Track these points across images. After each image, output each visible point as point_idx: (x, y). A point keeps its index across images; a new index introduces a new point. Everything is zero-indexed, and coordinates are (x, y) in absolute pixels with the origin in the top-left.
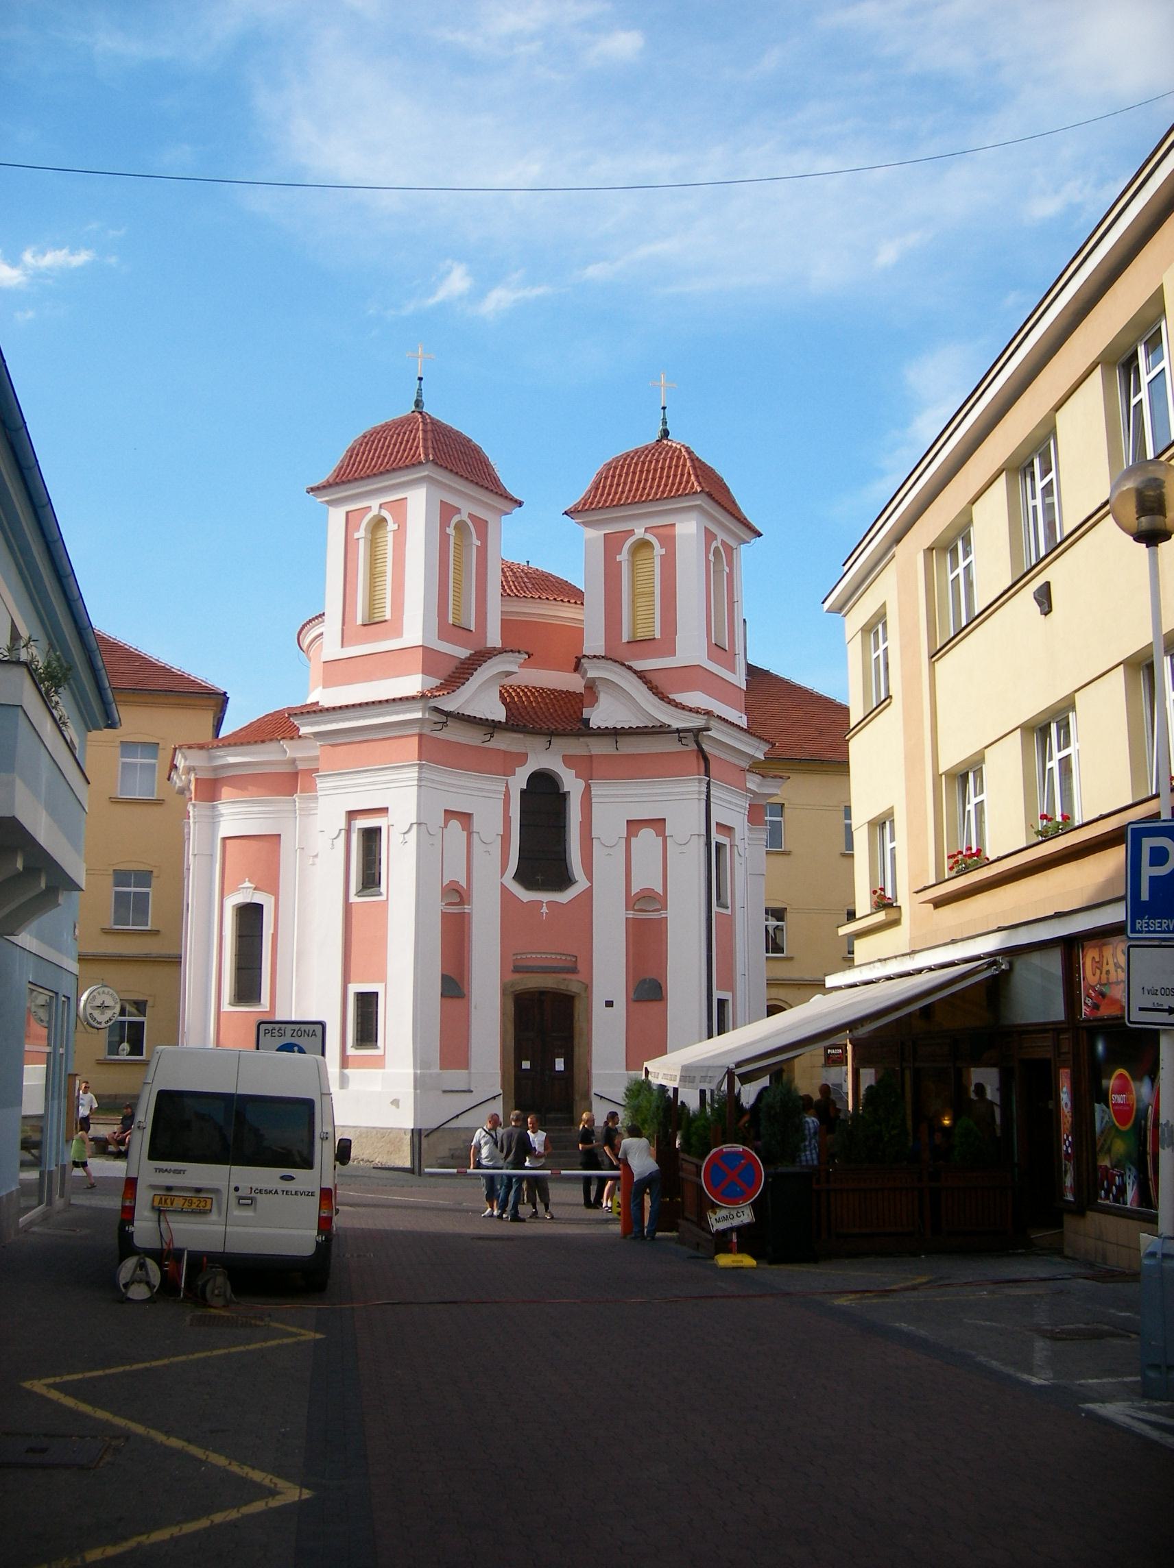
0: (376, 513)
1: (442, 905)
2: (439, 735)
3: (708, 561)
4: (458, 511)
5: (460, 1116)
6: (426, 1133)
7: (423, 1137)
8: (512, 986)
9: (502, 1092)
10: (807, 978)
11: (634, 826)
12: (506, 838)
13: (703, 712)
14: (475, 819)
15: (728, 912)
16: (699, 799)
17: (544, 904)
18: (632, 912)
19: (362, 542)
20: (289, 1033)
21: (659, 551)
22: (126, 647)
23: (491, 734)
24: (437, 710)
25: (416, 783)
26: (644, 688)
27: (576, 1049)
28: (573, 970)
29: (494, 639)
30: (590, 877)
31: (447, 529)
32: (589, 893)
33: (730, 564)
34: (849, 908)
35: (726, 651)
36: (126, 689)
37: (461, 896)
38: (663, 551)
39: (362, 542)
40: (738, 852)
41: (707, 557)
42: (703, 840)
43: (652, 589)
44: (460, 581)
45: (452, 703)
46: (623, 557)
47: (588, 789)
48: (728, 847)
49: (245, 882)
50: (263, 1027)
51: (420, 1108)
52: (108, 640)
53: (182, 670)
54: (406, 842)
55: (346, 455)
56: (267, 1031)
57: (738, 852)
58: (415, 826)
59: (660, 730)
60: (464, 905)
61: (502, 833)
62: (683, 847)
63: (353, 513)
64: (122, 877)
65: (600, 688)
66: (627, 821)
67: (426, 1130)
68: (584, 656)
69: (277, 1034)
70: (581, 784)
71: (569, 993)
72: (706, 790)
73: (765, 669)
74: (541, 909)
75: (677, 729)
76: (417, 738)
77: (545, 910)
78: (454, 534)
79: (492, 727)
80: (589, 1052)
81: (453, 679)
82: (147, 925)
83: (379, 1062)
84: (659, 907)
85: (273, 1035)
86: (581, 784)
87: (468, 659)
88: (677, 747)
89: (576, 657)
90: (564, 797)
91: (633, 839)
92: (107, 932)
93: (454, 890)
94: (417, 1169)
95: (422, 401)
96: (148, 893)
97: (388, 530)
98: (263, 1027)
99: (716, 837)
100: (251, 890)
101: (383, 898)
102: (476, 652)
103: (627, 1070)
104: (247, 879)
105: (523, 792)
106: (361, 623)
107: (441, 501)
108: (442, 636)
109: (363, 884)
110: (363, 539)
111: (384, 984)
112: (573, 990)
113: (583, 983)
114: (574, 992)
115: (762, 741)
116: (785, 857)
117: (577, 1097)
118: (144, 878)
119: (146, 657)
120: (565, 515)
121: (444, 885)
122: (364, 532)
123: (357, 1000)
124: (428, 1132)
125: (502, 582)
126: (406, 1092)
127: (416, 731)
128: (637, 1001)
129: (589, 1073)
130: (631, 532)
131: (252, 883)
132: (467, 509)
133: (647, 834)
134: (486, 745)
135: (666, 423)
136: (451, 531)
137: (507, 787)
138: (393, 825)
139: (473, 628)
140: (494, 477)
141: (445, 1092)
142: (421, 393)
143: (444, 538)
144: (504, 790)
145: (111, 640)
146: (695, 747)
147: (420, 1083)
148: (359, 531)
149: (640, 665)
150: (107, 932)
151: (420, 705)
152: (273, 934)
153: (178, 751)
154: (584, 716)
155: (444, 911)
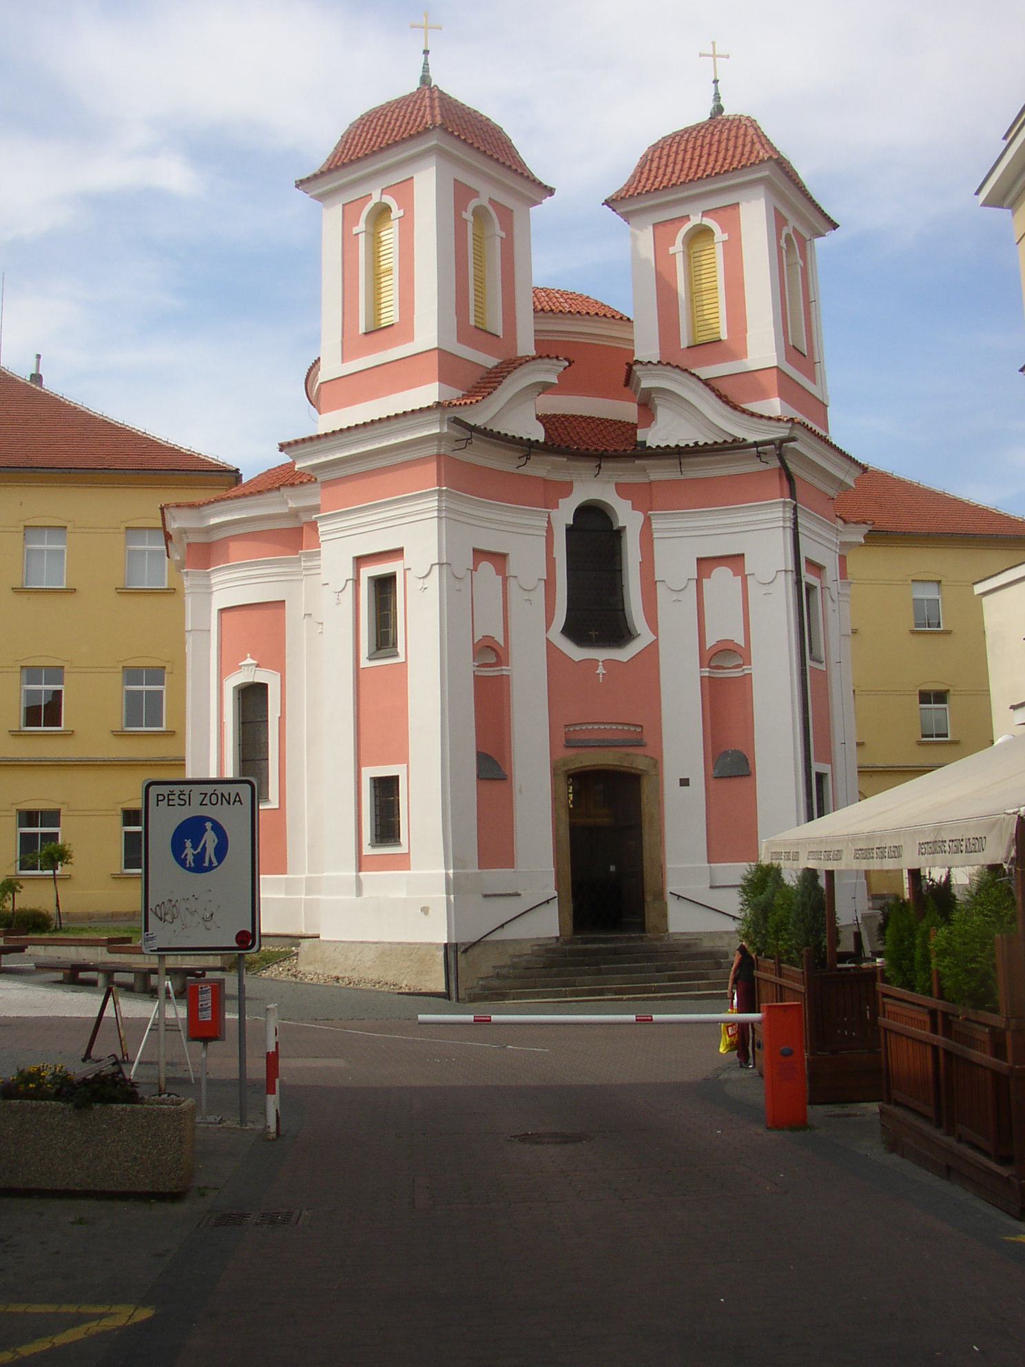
0: (378, 200)
1: (474, 665)
2: (459, 455)
3: (780, 248)
4: (475, 194)
5: (505, 926)
6: (463, 948)
8: (564, 764)
9: (557, 895)
11: (706, 564)
12: (550, 584)
13: (785, 419)
15: (369, 772)
16: (784, 527)
17: (600, 664)
18: (708, 669)
19: (362, 238)
20: (197, 799)
21: (720, 236)
22: (134, 431)
23: (527, 455)
24: (457, 421)
25: (436, 514)
26: (712, 398)
28: (640, 744)
29: (526, 346)
30: (656, 632)
31: (463, 213)
32: (653, 648)
33: (804, 257)
34: (922, 689)
35: (804, 356)
36: (129, 469)
37: (497, 655)
38: (725, 237)
40: (831, 598)
41: (778, 243)
42: (791, 578)
43: (714, 283)
45: (479, 417)
47: (648, 521)
48: (819, 589)
49: (246, 658)
50: (154, 790)
51: (456, 914)
52: (115, 426)
53: (192, 450)
54: (425, 588)
55: (341, 141)
56: (161, 798)
57: (831, 598)
58: (436, 568)
59: (733, 446)
61: (545, 578)
64: (132, 674)
65: (657, 401)
66: (700, 560)
67: (463, 944)
68: (637, 362)
69: (177, 801)
70: (639, 517)
75: (755, 442)
76: (434, 465)
77: (601, 670)
79: (528, 448)
80: (660, 843)
81: (477, 390)
82: (161, 726)
83: (403, 862)
84: (742, 663)
85: (171, 803)
86: (639, 517)
87: (496, 367)
89: (627, 364)
90: (618, 534)
91: (705, 580)
92: (118, 734)
93: (488, 647)
94: (453, 994)
95: (429, 76)
96: (162, 691)
97: (392, 218)
98: (154, 790)
99: (807, 577)
100: (254, 667)
101: (401, 659)
103: (709, 862)
104: (249, 655)
105: (569, 530)
106: (364, 331)
107: (455, 180)
108: (461, 339)
109: (377, 645)
110: (364, 234)
111: (406, 765)
113: (652, 758)
114: (641, 770)
115: (853, 465)
117: (649, 898)
118: (156, 675)
119: (155, 439)
120: (605, 206)
121: (476, 642)
122: (364, 225)
123: (375, 787)
124: (467, 946)
125: (534, 303)
126: (438, 897)
127: (434, 451)
129: (661, 868)
131: (254, 660)
132: (486, 193)
133: (722, 574)
134: (523, 471)
135: (720, 98)
136: (468, 215)
137: (549, 522)
138: (410, 569)
139: (500, 333)
140: (519, 161)
141: (486, 896)
142: (428, 69)
143: (460, 225)
144: (546, 525)
145: (119, 425)
146: (777, 464)
147: (455, 886)
148: (358, 224)
149: (706, 372)
150: (118, 734)
151: (437, 415)
153: (165, 510)
154: (639, 439)
155: (476, 674)
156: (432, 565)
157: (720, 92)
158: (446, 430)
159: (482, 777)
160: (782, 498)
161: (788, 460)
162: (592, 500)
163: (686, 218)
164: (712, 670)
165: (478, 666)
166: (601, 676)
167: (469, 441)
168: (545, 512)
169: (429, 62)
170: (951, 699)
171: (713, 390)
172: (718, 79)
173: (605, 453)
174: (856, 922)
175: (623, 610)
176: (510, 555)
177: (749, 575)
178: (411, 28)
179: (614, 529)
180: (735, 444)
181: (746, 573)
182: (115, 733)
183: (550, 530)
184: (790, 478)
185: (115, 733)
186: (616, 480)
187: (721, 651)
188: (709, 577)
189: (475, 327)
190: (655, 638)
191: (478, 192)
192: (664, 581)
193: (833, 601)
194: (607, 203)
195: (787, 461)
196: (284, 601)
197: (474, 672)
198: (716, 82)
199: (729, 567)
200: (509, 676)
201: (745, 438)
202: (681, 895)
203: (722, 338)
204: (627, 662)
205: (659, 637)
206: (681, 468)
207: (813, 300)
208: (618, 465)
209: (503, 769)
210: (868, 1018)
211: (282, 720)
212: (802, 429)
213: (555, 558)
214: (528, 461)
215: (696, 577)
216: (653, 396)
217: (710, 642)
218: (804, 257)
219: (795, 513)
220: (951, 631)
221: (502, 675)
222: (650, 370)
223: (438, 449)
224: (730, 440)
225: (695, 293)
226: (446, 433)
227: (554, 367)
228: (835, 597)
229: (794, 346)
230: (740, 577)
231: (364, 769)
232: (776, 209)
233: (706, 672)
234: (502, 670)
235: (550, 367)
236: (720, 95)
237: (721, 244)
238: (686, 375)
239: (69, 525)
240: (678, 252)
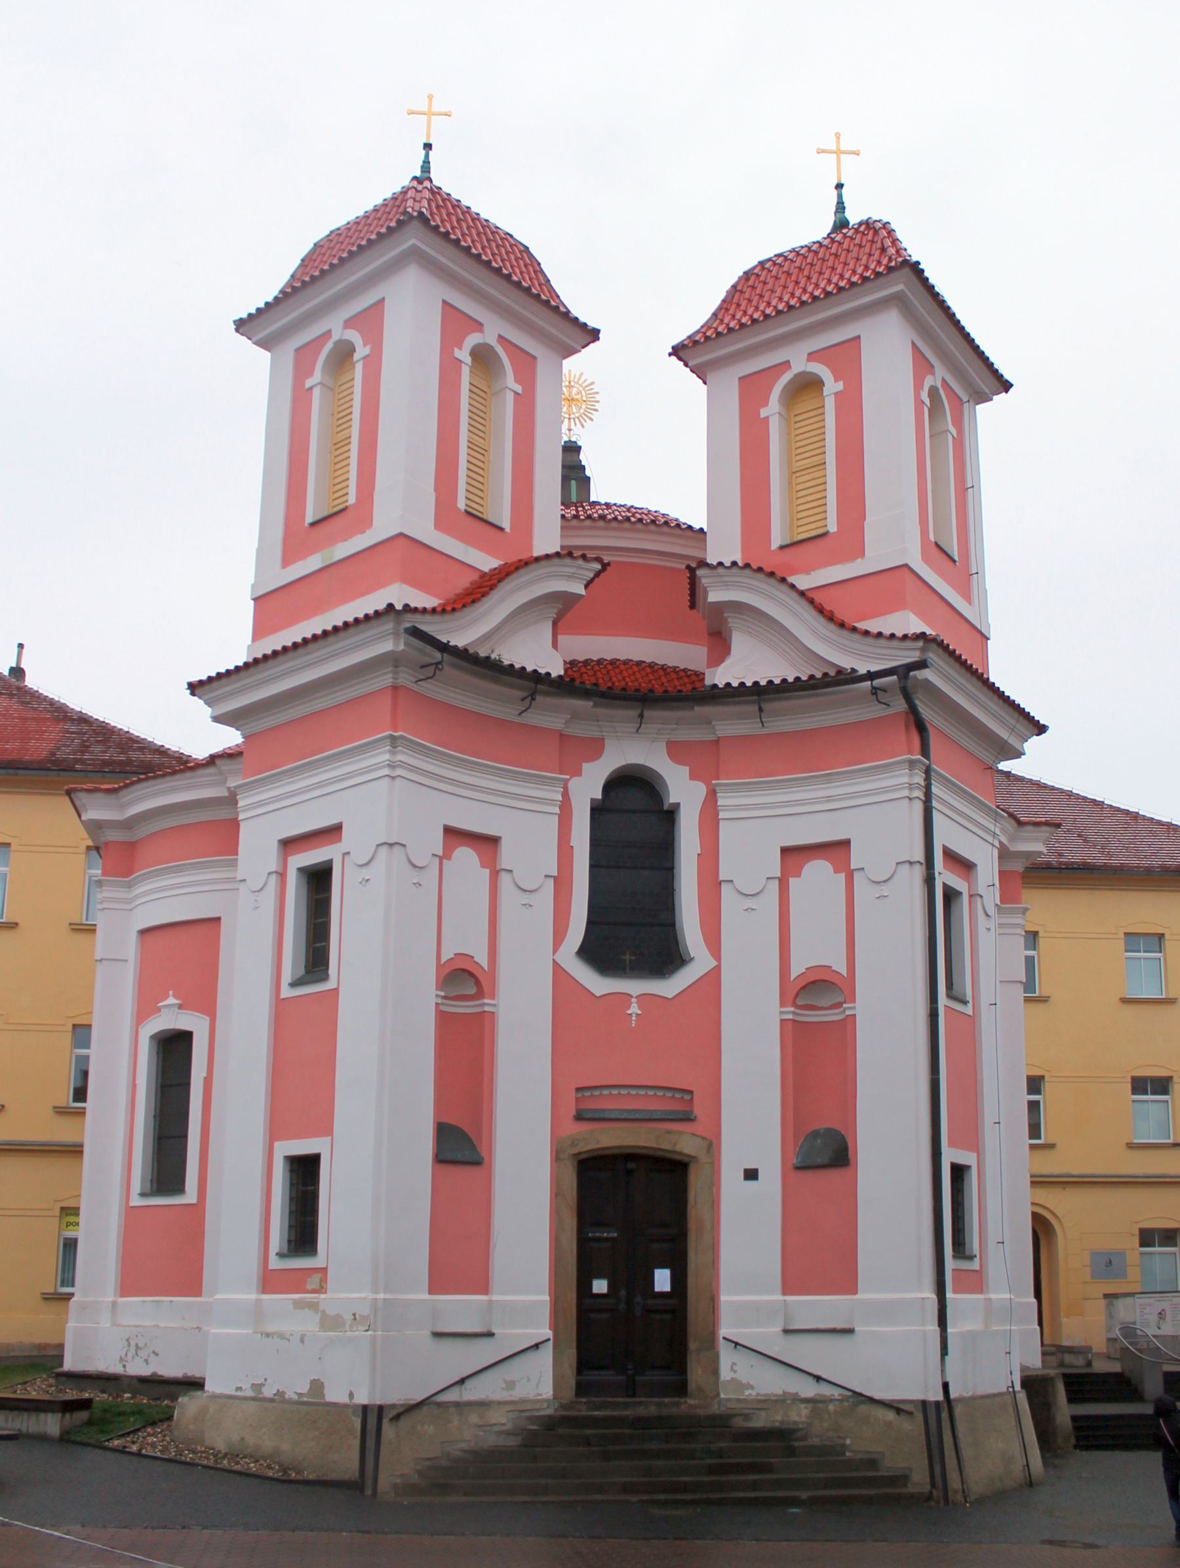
4: (479, 326)
6: (393, 1413)
8: (573, 1145)
10: (1074, 1172)
12: (562, 883)
14: (505, 848)
15: (975, 1265)
17: (634, 1000)
18: (792, 1009)
21: (832, 386)
24: (416, 633)
27: (691, 1255)
28: (687, 1118)
30: (717, 955)
31: (456, 350)
32: (713, 978)
35: (954, 561)
39: (316, 393)
42: (918, 872)
46: (772, 409)
47: (712, 795)
59: (845, 678)
60: (483, 997)
61: (556, 874)
63: (819, 1161)
66: (785, 851)
67: (393, 1406)
70: (700, 789)
72: (923, 783)
74: (629, 1009)
77: (634, 1009)
78: (470, 363)
80: (715, 1263)
84: (843, 1000)
86: (700, 789)
88: (874, 711)
90: (670, 816)
91: (793, 881)
99: (945, 876)
104: (171, 993)
105: (598, 811)
107: (445, 302)
108: (441, 523)
112: (685, 1151)
113: (703, 1138)
115: (1021, 718)
116: (1040, 1006)
117: (692, 1345)
128: (798, 1168)
129: (713, 1300)
130: (786, 365)
132: (493, 330)
133: (818, 870)
135: (844, 208)
137: (565, 794)
139: (506, 525)
141: (438, 1335)
149: (803, 582)
152: (205, 1078)
155: (442, 1008)
157: (844, 200)
158: (402, 647)
159: (441, 1159)
160: (908, 754)
161: (919, 699)
162: (631, 765)
163: (786, 365)
164: (798, 1011)
165: (445, 997)
166: (634, 1018)
167: (440, 666)
168: (559, 779)
169: (430, 160)
171: (811, 601)
172: (842, 182)
173: (649, 695)
174: (1011, 1390)
175: (673, 925)
177: (855, 870)
178: (409, 114)
180: (842, 677)
181: (852, 868)
182: (58, 1110)
184: (921, 727)
185: (58, 1110)
186: (668, 736)
187: (813, 982)
188: (799, 875)
189: (467, 512)
190: (715, 963)
191: (481, 325)
192: (732, 881)
193: (988, 915)
194: (677, 351)
195: (917, 702)
197: (437, 1004)
199: (826, 859)
200: (493, 1013)
201: (856, 668)
202: (740, 1342)
206: (761, 718)
207: (970, 485)
208: (668, 714)
209: (478, 1150)
211: (208, 1082)
212: (940, 651)
213: (572, 847)
215: (779, 875)
216: (725, 615)
217: (797, 969)
218: (958, 422)
219: (928, 779)
221: (484, 1011)
223: (394, 678)
224: (832, 673)
225: (794, 473)
226: (403, 650)
227: (581, 572)
229: (937, 544)
230: (843, 875)
231: (277, 1144)
232: (914, 344)
233: (789, 1012)
236: (845, 205)
237: (833, 396)
238: (784, 588)
239: (14, 842)
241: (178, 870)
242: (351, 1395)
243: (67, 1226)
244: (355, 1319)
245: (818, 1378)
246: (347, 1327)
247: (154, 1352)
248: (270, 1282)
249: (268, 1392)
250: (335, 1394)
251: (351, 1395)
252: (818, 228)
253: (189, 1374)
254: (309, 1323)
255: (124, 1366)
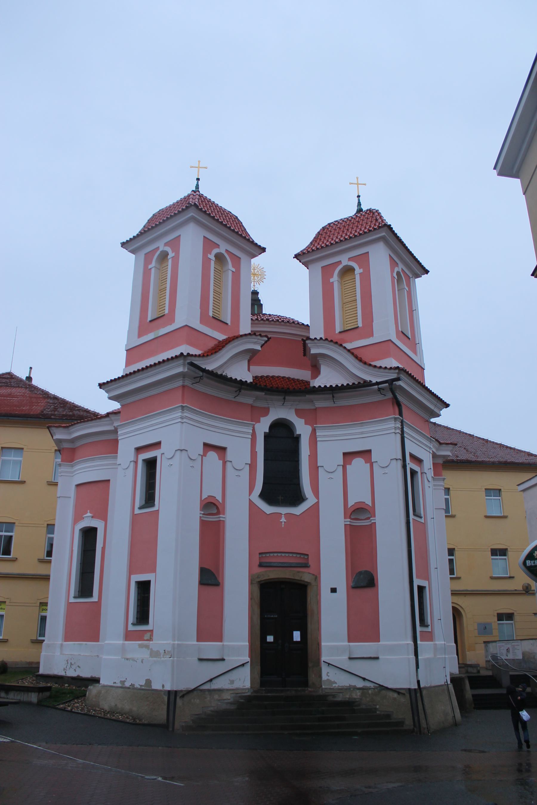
6: (181, 694)
7: (178, 698)
8: (258, 577)
10: (469, 589)
11: (348, 456)
12: (252, 467)
17: (283, 516)
18: (349, 520)
24: (192, 364)
27: (309, 626)
28: (306, 566)
32: (316, 506)
35: (409, 339)
38: (361, 271)
39: (153, 271)
42: (400, 463)
44: (221, 293)
47: (314, 431)
49: (87, 513)
62: (385, 469)
65: (321, 362)
66: (345, 454)
70: (309, 429)
71: (303, 583)
72: (400, 427)
73: (433, 422)
74: (281, 519)
77: (283, 520)
80: (319, 629)
84: (370, 516)
86: (309, 429)
90: (297, 439)
91: (348, 466)
102: (229, 337)
104: (88, 511)
105: (267, 437)
110: (154, 268)
112: (306, 580)
113: (313, 575)
115: (439, 401)
117: (310, 665)
128: (354, 588)
129: (319, 645)
130: (340, 262)
132: (223, 247)
133: (358, 462)
136: (212, 256)
137: (254, 430)
138: (164, 453)
139: (229, 322)
149: (349, 346)
151: (181, 361)
152: (102, 547)
155: (203, 519)
156: (176, 451)
158: (186, 370)
159: (202, 583)
163: (340, 262)
166: (283, 523)
167: (202, 378)
169: (199, 184)
170: (509, 553)
171: (352, 354)
172: (360, 195)
174: (446, 683)
176: (228, 448)
179: (295, 436)
183: (254, 435)
184: (399, 404)
186: (295, 407)
189: (213, 317)
190: (317, 501)
193: (429, 481)
194: (297, 256)
196: (109, 481)
198: (359, 196)
200: (224, 521)
202: (330, 663)
203: (360, 326)
204: (299, 515)
205: (320, 500)
206: (333, 400)
210: (515, 706)
211: (103, 549)
212: (405, 374)
213: (256, 452)
214: (240, 393)
215: (342, 464)
218: (409, 285)
220: (507, 516)
222: (315, 343)
226: (187, 371)
228: (430, 479)
229: (402, 332)
231: (132, 576)
232: (390, 255)
234: (220, 517)
235: (256, 340)
237: (359, 274)
240: (335, 281)
241: (93, 460)
242: (163, 686)
243: (42, 611)
244: (165, 653)
245: (364, 679)
246: (162, 656)
247: (78, 666)
248: (129, 636)
249: (127, 684)
250: (156, 686)
251: (163, 686)
252: (351, 211)
253: (93, 676)
254: (144, 654)
255: (65, 672)
